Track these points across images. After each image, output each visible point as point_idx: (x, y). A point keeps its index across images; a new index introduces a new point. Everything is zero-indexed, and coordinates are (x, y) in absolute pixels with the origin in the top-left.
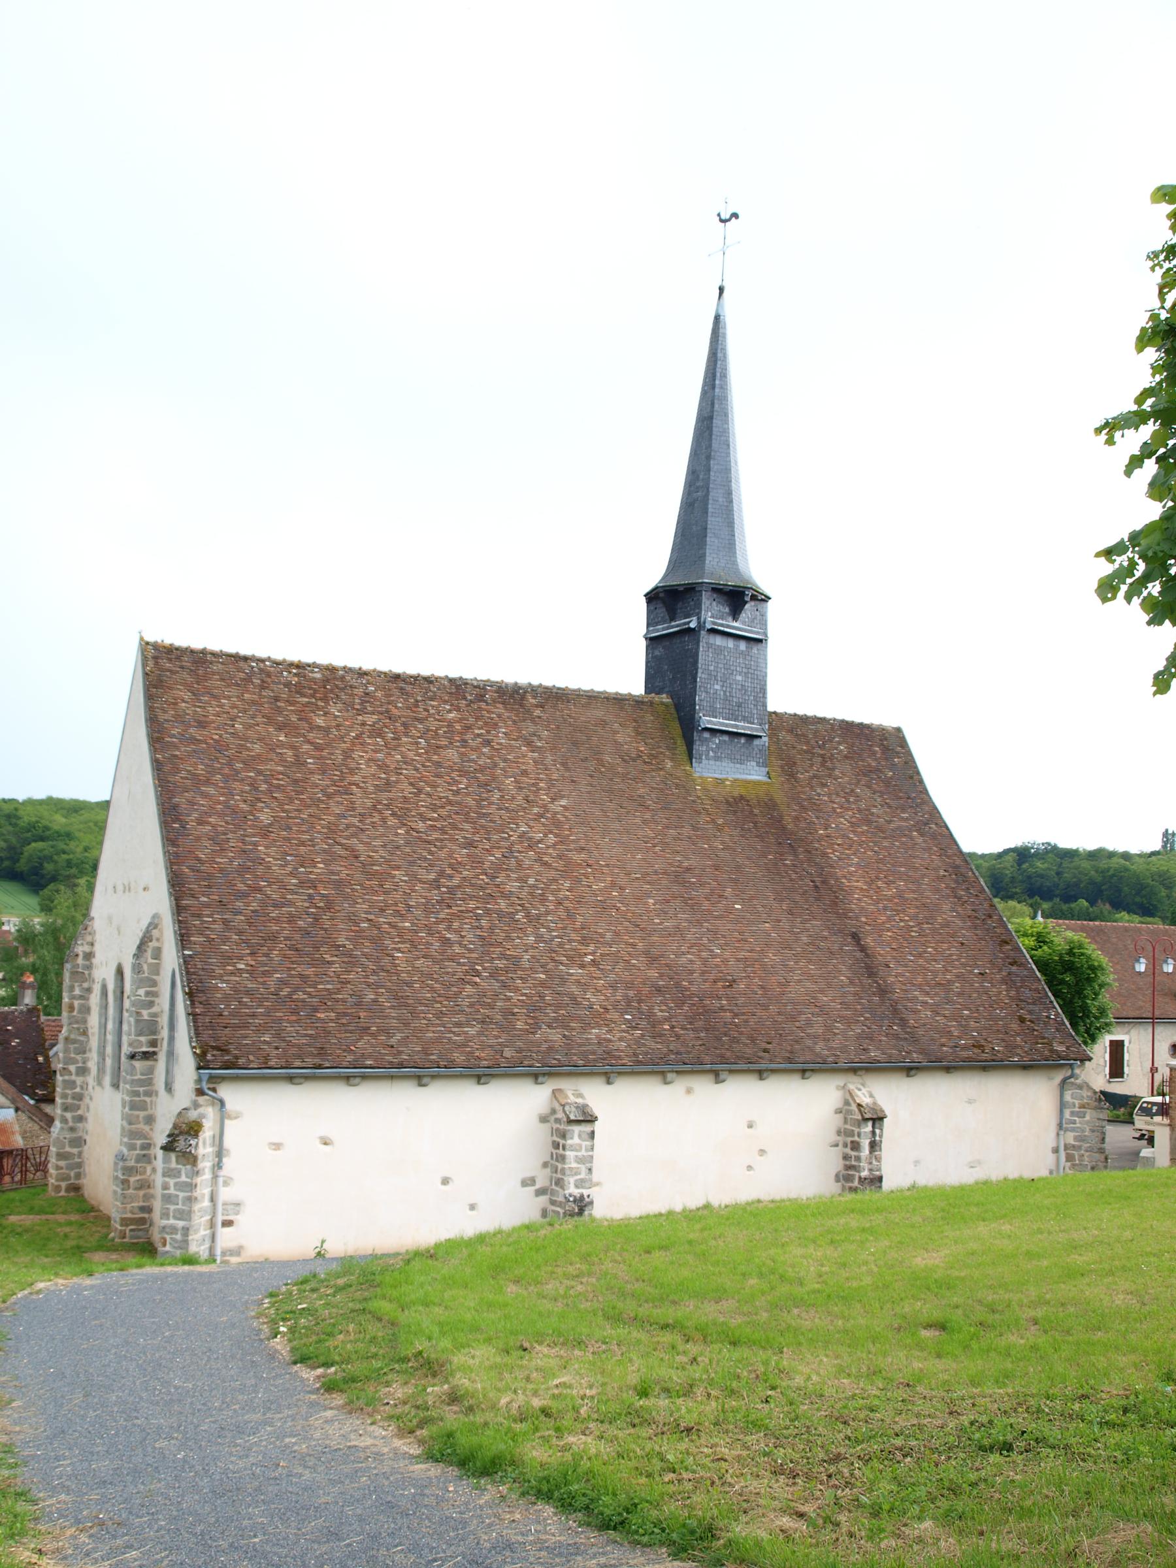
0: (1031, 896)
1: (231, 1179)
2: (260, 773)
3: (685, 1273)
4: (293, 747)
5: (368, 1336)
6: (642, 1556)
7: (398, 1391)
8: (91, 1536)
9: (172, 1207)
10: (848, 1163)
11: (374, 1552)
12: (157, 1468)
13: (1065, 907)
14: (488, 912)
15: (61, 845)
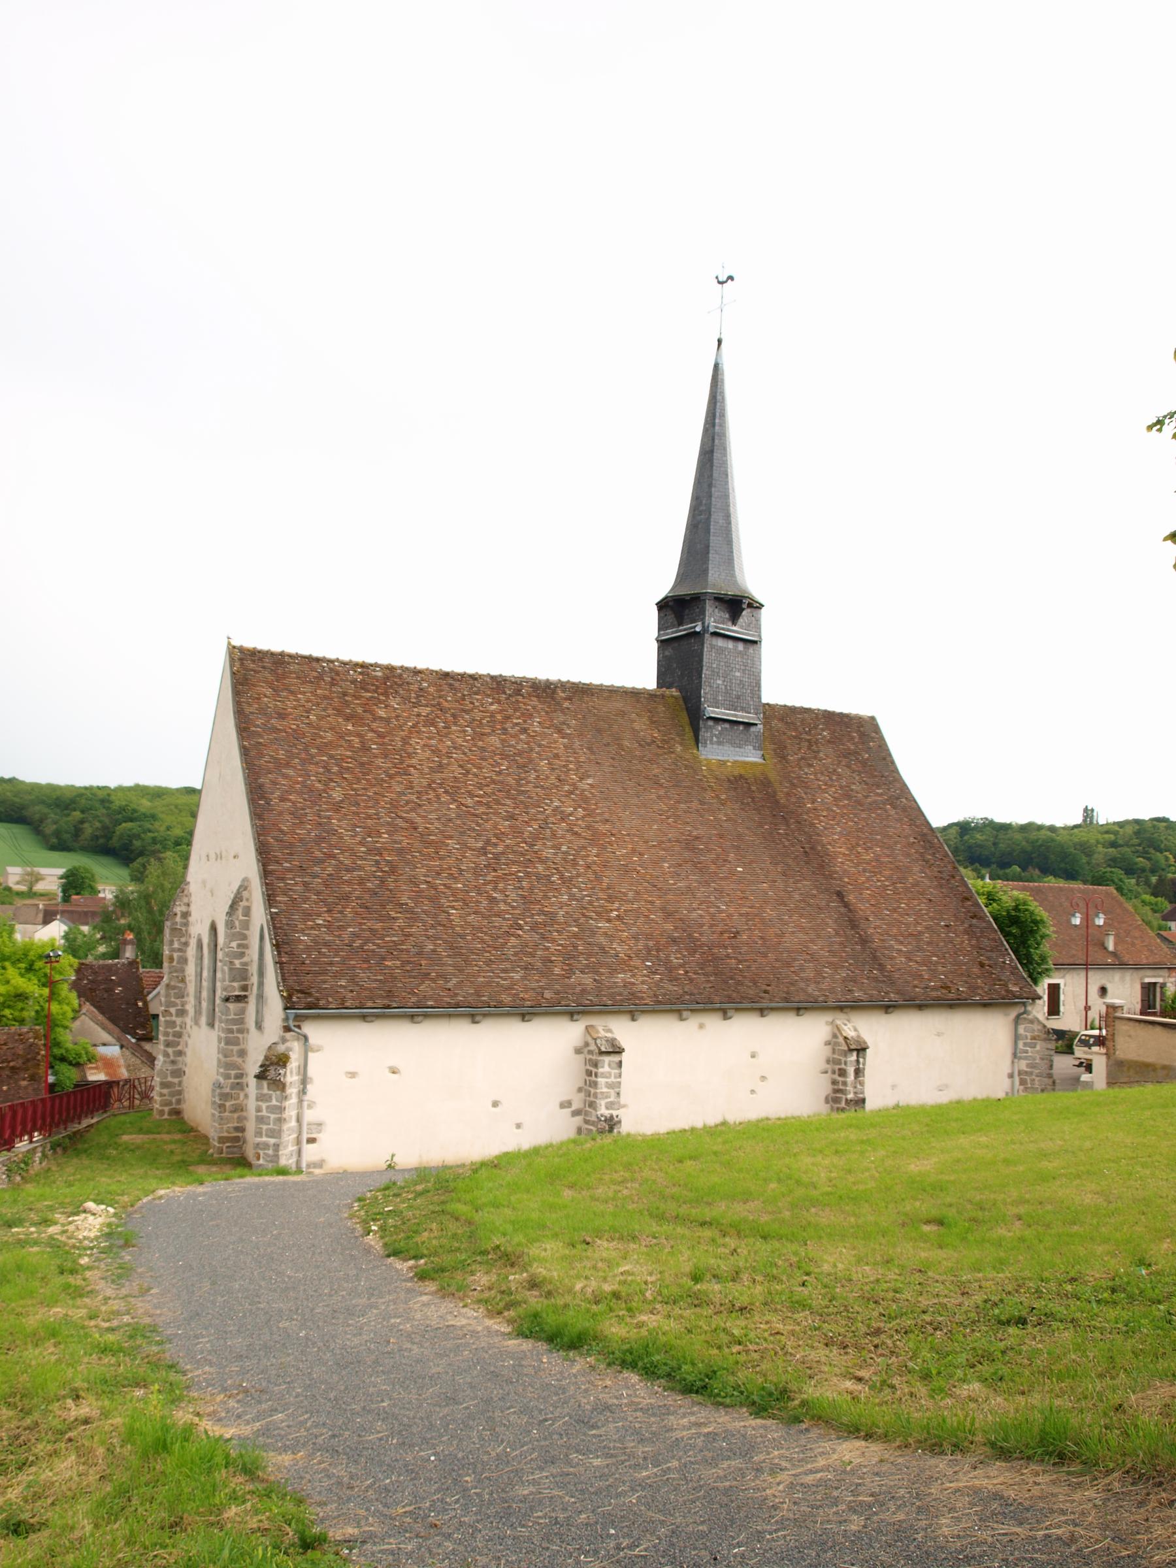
0: (972, 863)
1: (314, 1103)
2: (331, 757)
3: (716, 1179)
4: (359, 735)
5: (450, 1234)
6: (726, 1415)
7: (482, 1279)
8: (238, 1401)
9: (265, 1127)
10: (836, 1087)
11: (491, 1414)
12: (284, 1344)
13: (1001, 872)
14: (528, 874)
15: (147, 825)
